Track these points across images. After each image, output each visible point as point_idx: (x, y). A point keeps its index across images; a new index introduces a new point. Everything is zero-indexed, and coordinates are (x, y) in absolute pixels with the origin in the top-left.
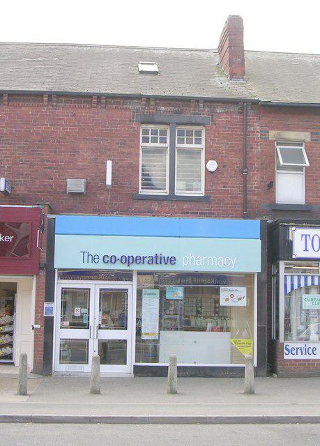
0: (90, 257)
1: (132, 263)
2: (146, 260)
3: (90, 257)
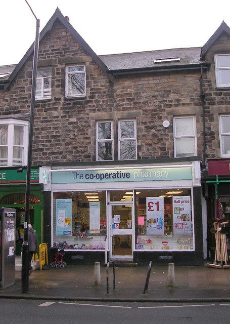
0: (78, 176)
1: (103, 178)
2: (111, 176)
3: (78, 176)
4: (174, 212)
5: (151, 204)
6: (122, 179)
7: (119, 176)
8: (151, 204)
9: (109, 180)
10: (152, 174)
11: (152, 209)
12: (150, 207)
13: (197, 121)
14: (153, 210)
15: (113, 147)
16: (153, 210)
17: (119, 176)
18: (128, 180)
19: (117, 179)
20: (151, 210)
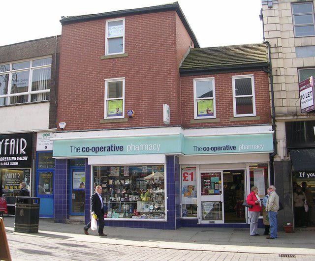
0: (75, 149)
2: (106, 149)
3: (75, 149)
4: (166, 198)
5: (186, 174)
6: (116, 152)
7: (113, 149)
8: (186, 174)
9: (103, 153)
10: (144, 148)
11: (187, 179)
12: (185, 177)
13: (233, 75)
14: (188, 180)
15: (305, 135)
16: (188, 180)
17: (113, 149)
18: (235, 151)
19: (111, 152)
20: (186, 180)
